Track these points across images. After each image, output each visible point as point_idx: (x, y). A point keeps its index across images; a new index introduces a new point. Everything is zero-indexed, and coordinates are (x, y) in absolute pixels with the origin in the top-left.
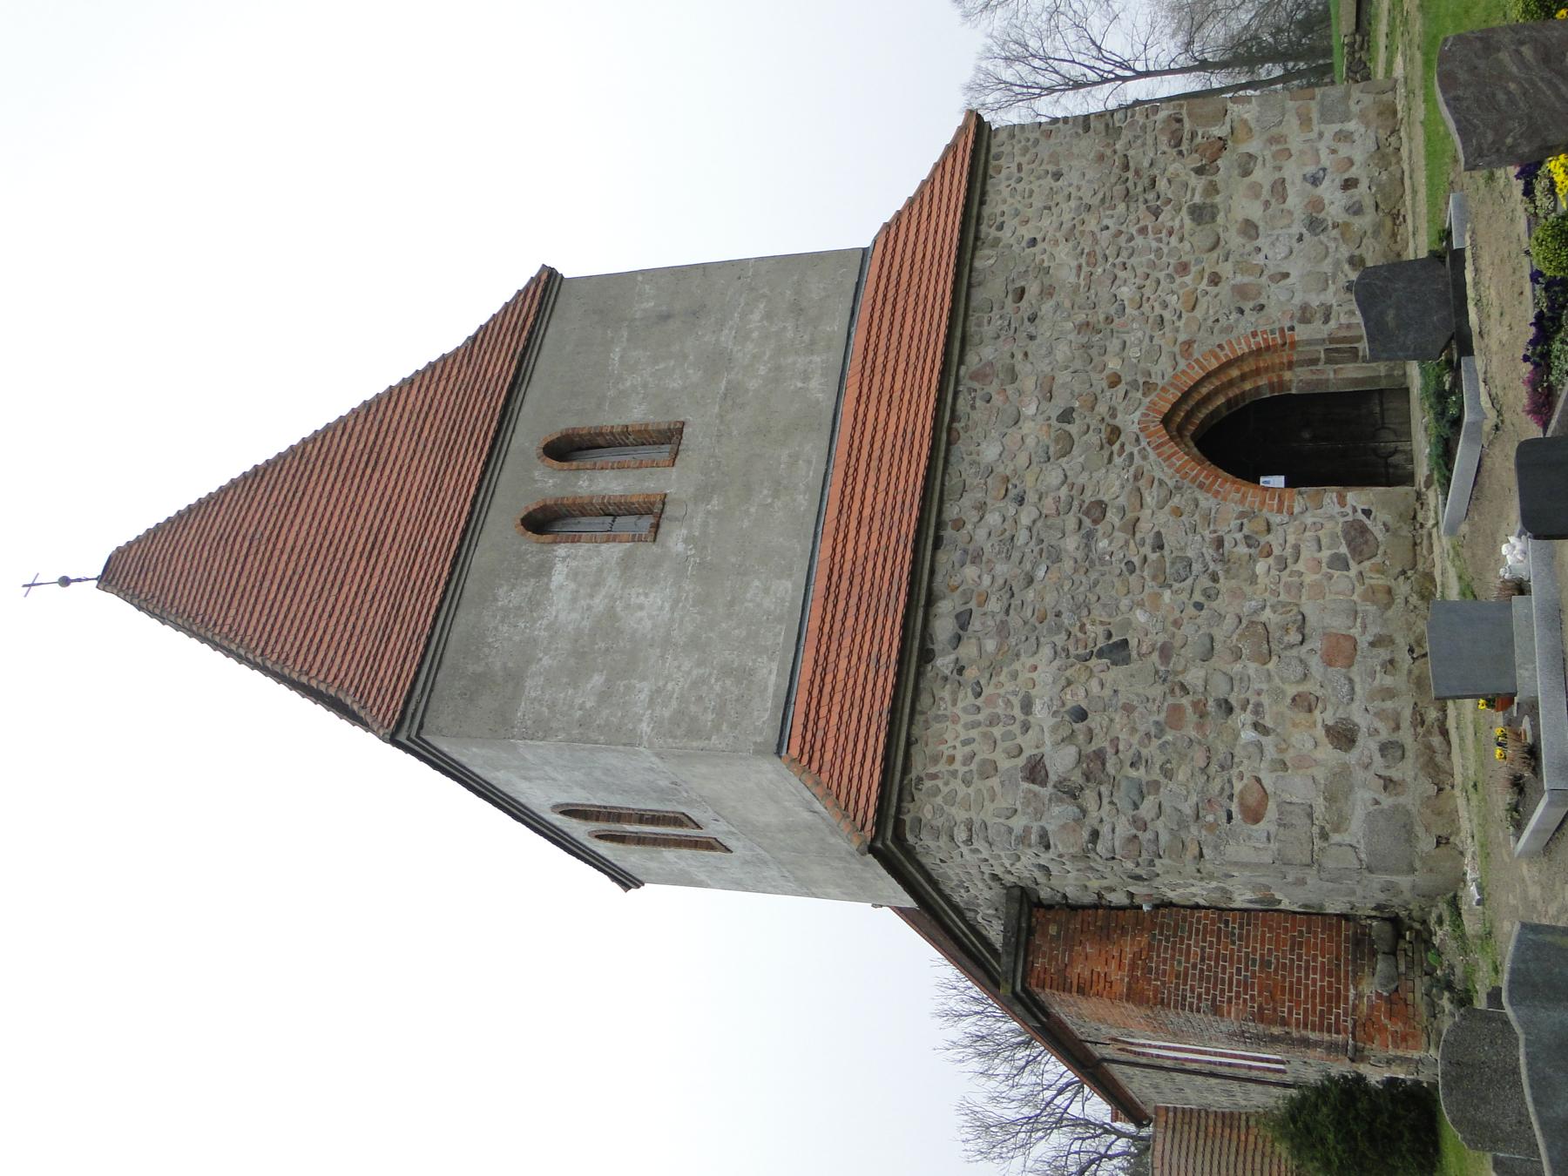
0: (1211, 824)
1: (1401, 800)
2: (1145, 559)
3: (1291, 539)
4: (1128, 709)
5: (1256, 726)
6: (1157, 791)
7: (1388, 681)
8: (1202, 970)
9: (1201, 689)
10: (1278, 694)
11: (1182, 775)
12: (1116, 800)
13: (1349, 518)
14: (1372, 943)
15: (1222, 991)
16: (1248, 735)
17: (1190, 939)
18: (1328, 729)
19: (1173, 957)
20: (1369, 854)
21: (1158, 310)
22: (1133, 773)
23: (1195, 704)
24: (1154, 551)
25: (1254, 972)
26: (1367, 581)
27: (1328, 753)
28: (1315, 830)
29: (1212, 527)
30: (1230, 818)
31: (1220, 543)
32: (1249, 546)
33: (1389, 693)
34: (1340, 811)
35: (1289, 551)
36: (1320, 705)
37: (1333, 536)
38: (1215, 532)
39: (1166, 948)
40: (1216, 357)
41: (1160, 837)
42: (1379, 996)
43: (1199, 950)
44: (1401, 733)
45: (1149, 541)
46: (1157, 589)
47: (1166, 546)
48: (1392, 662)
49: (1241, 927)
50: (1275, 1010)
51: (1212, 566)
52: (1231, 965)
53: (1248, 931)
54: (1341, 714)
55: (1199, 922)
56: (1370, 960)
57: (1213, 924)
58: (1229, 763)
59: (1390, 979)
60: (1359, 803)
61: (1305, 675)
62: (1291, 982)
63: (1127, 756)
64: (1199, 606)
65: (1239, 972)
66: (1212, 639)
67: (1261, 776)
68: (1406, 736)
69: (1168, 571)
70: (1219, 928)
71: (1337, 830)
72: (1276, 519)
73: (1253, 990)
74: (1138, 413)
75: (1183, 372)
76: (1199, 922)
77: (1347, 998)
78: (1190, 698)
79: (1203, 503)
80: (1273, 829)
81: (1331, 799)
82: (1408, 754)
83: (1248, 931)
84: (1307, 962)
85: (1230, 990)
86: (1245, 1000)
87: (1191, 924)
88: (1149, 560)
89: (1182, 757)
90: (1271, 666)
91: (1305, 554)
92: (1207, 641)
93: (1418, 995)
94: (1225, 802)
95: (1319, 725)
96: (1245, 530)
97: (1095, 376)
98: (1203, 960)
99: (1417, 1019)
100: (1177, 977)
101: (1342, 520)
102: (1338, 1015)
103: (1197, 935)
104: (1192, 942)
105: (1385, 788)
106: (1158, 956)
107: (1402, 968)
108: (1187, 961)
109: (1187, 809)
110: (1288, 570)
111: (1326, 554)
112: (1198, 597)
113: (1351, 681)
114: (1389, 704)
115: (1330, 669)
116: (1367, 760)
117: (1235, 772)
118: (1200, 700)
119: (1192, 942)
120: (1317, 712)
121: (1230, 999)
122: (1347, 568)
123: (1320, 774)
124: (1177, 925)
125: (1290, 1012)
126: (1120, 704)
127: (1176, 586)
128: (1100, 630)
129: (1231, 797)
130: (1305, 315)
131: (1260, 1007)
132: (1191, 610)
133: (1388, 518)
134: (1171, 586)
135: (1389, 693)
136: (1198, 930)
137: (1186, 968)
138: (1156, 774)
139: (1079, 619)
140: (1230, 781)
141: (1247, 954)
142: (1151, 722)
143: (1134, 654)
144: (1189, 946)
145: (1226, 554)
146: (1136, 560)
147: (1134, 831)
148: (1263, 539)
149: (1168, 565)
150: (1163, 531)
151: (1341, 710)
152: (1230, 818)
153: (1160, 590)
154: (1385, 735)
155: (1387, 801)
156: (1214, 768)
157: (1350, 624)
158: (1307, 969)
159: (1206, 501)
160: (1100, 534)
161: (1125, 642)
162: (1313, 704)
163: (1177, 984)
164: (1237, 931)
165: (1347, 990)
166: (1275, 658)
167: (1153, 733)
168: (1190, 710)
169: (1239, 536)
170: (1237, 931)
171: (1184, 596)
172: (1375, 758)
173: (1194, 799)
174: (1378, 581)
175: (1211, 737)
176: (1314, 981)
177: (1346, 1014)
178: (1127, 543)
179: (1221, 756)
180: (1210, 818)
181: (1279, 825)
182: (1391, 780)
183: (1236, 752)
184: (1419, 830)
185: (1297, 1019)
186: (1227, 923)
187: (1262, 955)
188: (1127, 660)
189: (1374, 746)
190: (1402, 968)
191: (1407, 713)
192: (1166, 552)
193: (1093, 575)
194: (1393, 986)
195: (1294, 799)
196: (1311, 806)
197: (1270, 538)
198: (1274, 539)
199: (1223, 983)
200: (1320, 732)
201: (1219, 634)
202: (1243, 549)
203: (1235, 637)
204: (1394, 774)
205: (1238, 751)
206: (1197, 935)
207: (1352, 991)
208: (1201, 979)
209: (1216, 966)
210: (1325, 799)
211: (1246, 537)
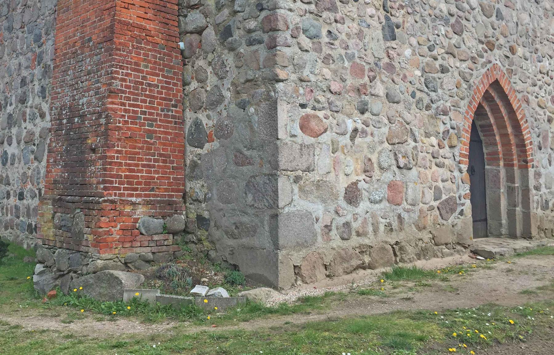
0: (298, 91)
1: (320, 239)
2: (436, 59)
3: (447, 162)
4: (360, 35)
5: (356, 130)
6: (315, 50)
7: (382, 228)
8: (142, 84)
9: (373, 92)
10: (371, 148)
11: (326, 72)
12: (308, 14)
13: (458, 201)
14: (170, 215)
15: (128, 99)
16: (350, 125)
17: (163, 76)
18: (355, 184)
19: (150, 62)
20: (288, 214)
21: (539, 83)
22: (324, 32)
23: (364, 85)
24: (441, 66)
25: (144, 125)
26: (429, 212)
27: (342, 184)
28: (300, 173)
29: (452, 108)
30: (303, 106)
31: (445, 113)
32: (444, 132)
33: (376, 231)
34: (311, 192)
35: (441, 160)
36: (368, 179)
37: (449, 190)
38: (450, 109)
39: (155, 57)
40: (522, 119)
41: (287, 49)
42: (136, 220)
43: (156, 82)
44: (355, 237)
45: (445, 63)
46: (421, 65)
47: (444, 75)
48: (392, 230)
49: (174, 117)
50: (119, 140)
51: (434, 106)
52: (146, 107)
53: (170, 122)
54: (365, 194)
55: (175, 85)
56: (160, 213)
57: (175, 95)
58: (334, 109)
59: (148, 229)
60: (316, 206)
61: (383, 168)
62: (138, 153)
63: (334, 27)
64: (413, 95)
65: (144, 113)
66: (398, 103)
67: (328, 132)
68: (355, 241)
69: (430, 75)
70: (171, 100)
71: (301, 189)
72: (457, 151)
73: (132, 123)
74: (500, 64)
75: (516, 97)
76: (175, 85)
77: (132, 195)
78: (368, 83)
79: (462, 103)
80: (299, 140)
81: (318, 185)
82: (345, 242)
83: (170, 122)
84: (154, 166)
85: (130, 105)
86: (123, 116)
87: (173, 78)
88: (435, 62)
89: (335, 72)
90: (386, 145)
91: (441, 170)
92: (396, 100)
93: (138, 250)
94: (312, 103)
95: (357, 178)
96: (451, 131)
97: (514, 37)
98: (149, 85)
99: (123, 250)
100: (137, 64)
101: (457, 196)
102: (119, 189)
103: (167, 82)
104: (160, 78)
105: (326, 226)
106: (150, 50)
107: (156, 238)
108: (148, 73)
109: (306, 73)
110: (432, 159)
111: (440, 184)
112: (418, 94)
113: (381, 201)
114: (370, 229)
115: (386, 186)
116: (341, 212)
117: (329, 113)
118: (366, 90)
119: (160, 78)
120: (364, 176)
121: (124, 104)
122: (435, 200)
123: (331, 177)
124: (172, 67)
125: (118, 152)
126: (362, 28)
127: (423, 80)
128: (400, 20)
129: (314, 108)
130: (538, 175)
131: (120, 128)
132: (411, 89)
133: (459, 227)
134: (422, 76)
135: (376, 231)
136: (169, 83)
137: (142, 72)
138: (326, 50)
139: (406, 6)
140: (323, 108)
141: (156, 120)
142: (354, 51)
143: (389, 44)
144: (158, 75)
145: (439, 116)
146: (435, 53)
147: (291, 27)
148: (446, 142)
149: (433, 75)
150: (450, 74)
151: (366, 194)
152: (303, 106)
153: (420, 68)
154: (355, 225)
155: (318, 227)
156: (329, 95)
157: (409, 202)
158: (149, 166)
159: (463, 104)
160: (447, 29)
161: (394, 39)
162: (367, 174)
163: (130, 63)
164: (170, 113)
165: (138, 196)
166: (390, 147)
167: (348, 51)
168: (362, 82)
169: (448, 126)
170: (170, 113)
171: (418, 85)
172: (342, 218)
173: (313, 78)
174: (429, 220)
175: (347, 96)
176: (141, 171)
177: (121, 195)
178: (443, 47)
179: (338, 103)
180: (301, 91)
181: (301, 145)
182: (330, 230)
183: (340, 114)
184: (303, 252)
185: (114, 157)
186: (175, 106)
187: (155, 132)
188: (385, 39)
189: (349, 218)
190: (156, 238)
191: (366, 241)
192: (440, 75)
193: (428, 19)
194: (143, 231)
195: (316, 157)
196: (313, 170)
197: (447, 147)
198: (446, 151)
199: (136, 100)
200: (354, 178)
201: (400, 107)
202: (442, 128)
203: (401, 119)
204: (334, 232)
205: (340, 116)
206: (167, 82)
207: (139, 200)
208: (136, 83)
209: (146, 96)
210: (319, 181)
211: (448, 131)
